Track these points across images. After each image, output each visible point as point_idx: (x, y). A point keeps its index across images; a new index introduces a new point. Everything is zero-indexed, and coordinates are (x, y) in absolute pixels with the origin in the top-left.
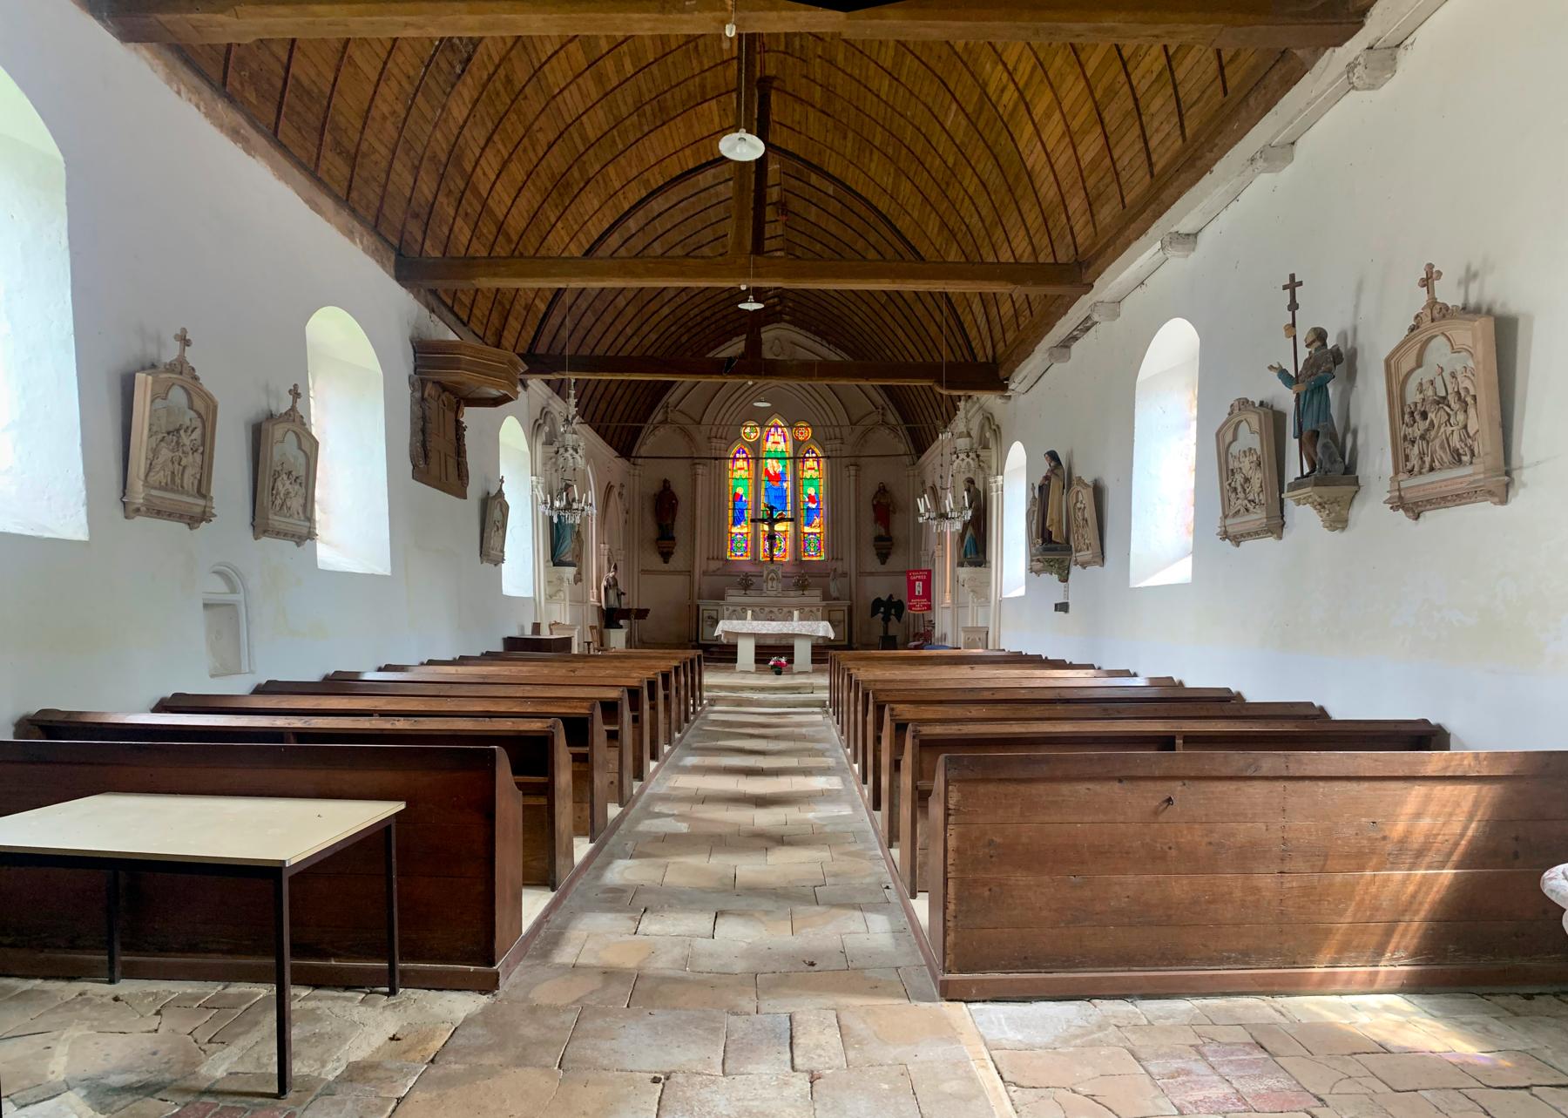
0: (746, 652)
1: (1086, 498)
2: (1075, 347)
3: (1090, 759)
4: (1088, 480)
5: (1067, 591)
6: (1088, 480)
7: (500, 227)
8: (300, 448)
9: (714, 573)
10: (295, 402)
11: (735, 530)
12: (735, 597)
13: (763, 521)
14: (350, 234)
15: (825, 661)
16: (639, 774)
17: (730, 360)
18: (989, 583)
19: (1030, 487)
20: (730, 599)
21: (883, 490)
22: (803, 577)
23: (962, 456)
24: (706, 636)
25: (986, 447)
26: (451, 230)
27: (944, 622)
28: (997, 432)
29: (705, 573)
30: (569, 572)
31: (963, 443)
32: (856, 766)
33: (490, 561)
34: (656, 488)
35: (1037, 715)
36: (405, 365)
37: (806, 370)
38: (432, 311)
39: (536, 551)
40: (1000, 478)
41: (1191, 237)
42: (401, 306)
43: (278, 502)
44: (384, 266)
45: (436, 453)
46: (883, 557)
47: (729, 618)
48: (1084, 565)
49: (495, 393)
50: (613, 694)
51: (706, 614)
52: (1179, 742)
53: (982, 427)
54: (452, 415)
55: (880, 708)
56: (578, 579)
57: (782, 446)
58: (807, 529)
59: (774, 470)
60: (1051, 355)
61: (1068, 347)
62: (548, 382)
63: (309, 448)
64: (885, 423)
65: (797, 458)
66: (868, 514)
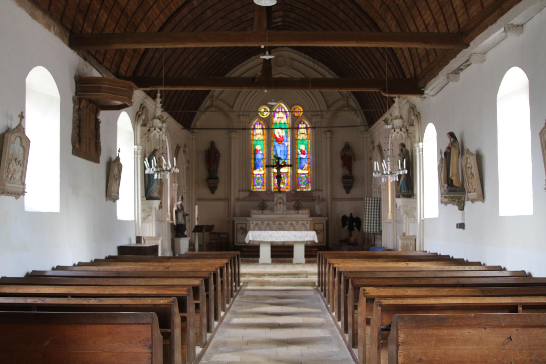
0: (265, 253)
1: (472, 161)
2: (462, 74)
3: (470, 318)
4: (473, 150)
5: (463, 215)
6: (473, 150)
7: (123, 11)
8: (22, 145)
9: (243, 200)
10: (21, 120)
11: (255, 172)
12: (257, 216)
13: (273, 166)
14: (48, 27)
15: (315, 256)
16: (209, 330)
17: (254, 78)
18: (416, 208)
19: (440, 152)
20: (254, 216)
21: (347, 147)
22: (298, 200)
23: (397, 130)
24: (238, 241)
25: (412, 125)
26: (98, 16)
27: (389, 240)
28: (418, 116)
29: (238, 200)
30: (156, 203)
31: (398, 123)
32: (340, 323)
33: (110, 199)
34: (206, 146)
35: (445, 294)
36: (71, 92)
37: (304, 83)
38: (86, 59)
39: (136, 190)
40: (421, 144)
41: (520, 27)
42: (70, 58)
43: (10, 176)
44: (63, 40)
45: (85, 139)
46: (348, 188)
47: (254, 230)
48: (473, 201)
49: (119, 103)
50: (196, 282)
51: (239, 226)
52: (520, 309)
53: (409, 112)
54: (93, 116)
55: (357, 289)
56: (160, 207)
57: (284, 120)
58: (300, 171)
59: (281, 137)
60: (448, 77)
61: (458, 74)
62: (144, 91)
63: (25, 143)
64: (348, 106)
65: (294, 128)
66: (338, 162)
